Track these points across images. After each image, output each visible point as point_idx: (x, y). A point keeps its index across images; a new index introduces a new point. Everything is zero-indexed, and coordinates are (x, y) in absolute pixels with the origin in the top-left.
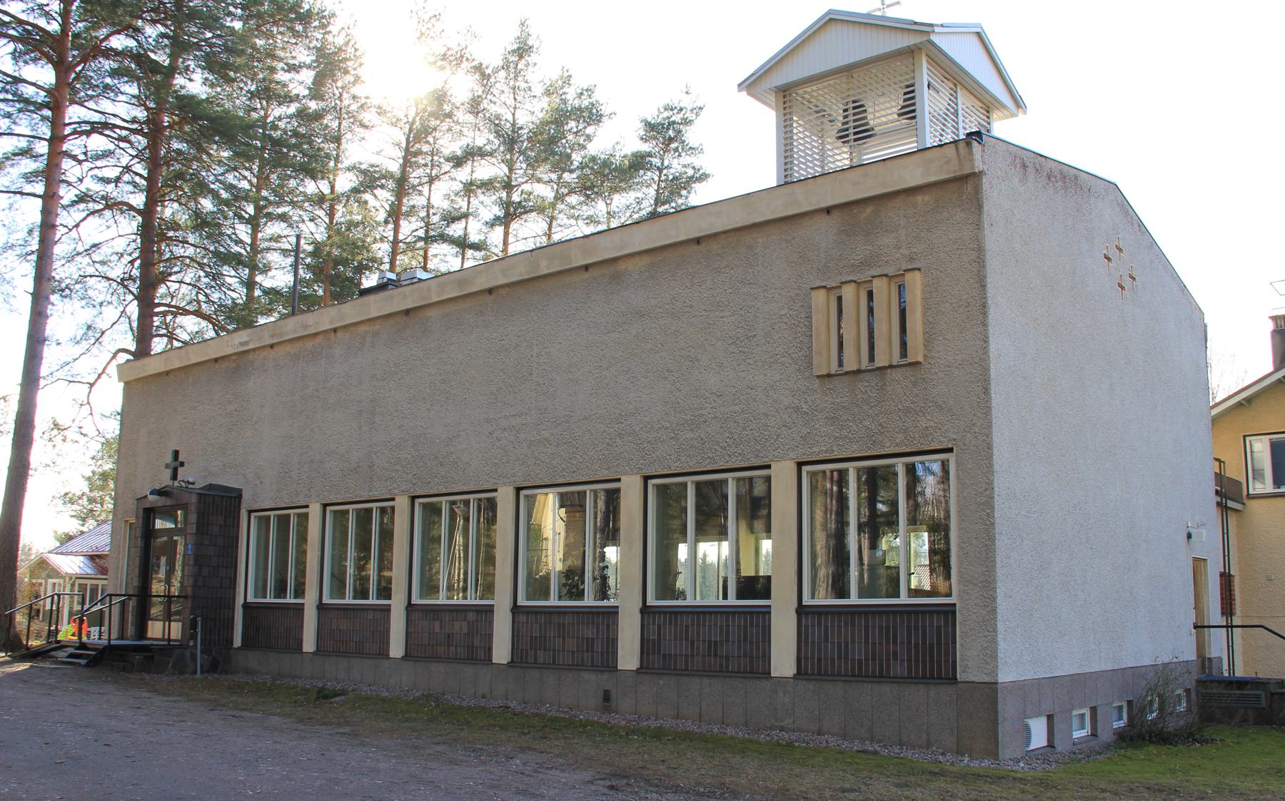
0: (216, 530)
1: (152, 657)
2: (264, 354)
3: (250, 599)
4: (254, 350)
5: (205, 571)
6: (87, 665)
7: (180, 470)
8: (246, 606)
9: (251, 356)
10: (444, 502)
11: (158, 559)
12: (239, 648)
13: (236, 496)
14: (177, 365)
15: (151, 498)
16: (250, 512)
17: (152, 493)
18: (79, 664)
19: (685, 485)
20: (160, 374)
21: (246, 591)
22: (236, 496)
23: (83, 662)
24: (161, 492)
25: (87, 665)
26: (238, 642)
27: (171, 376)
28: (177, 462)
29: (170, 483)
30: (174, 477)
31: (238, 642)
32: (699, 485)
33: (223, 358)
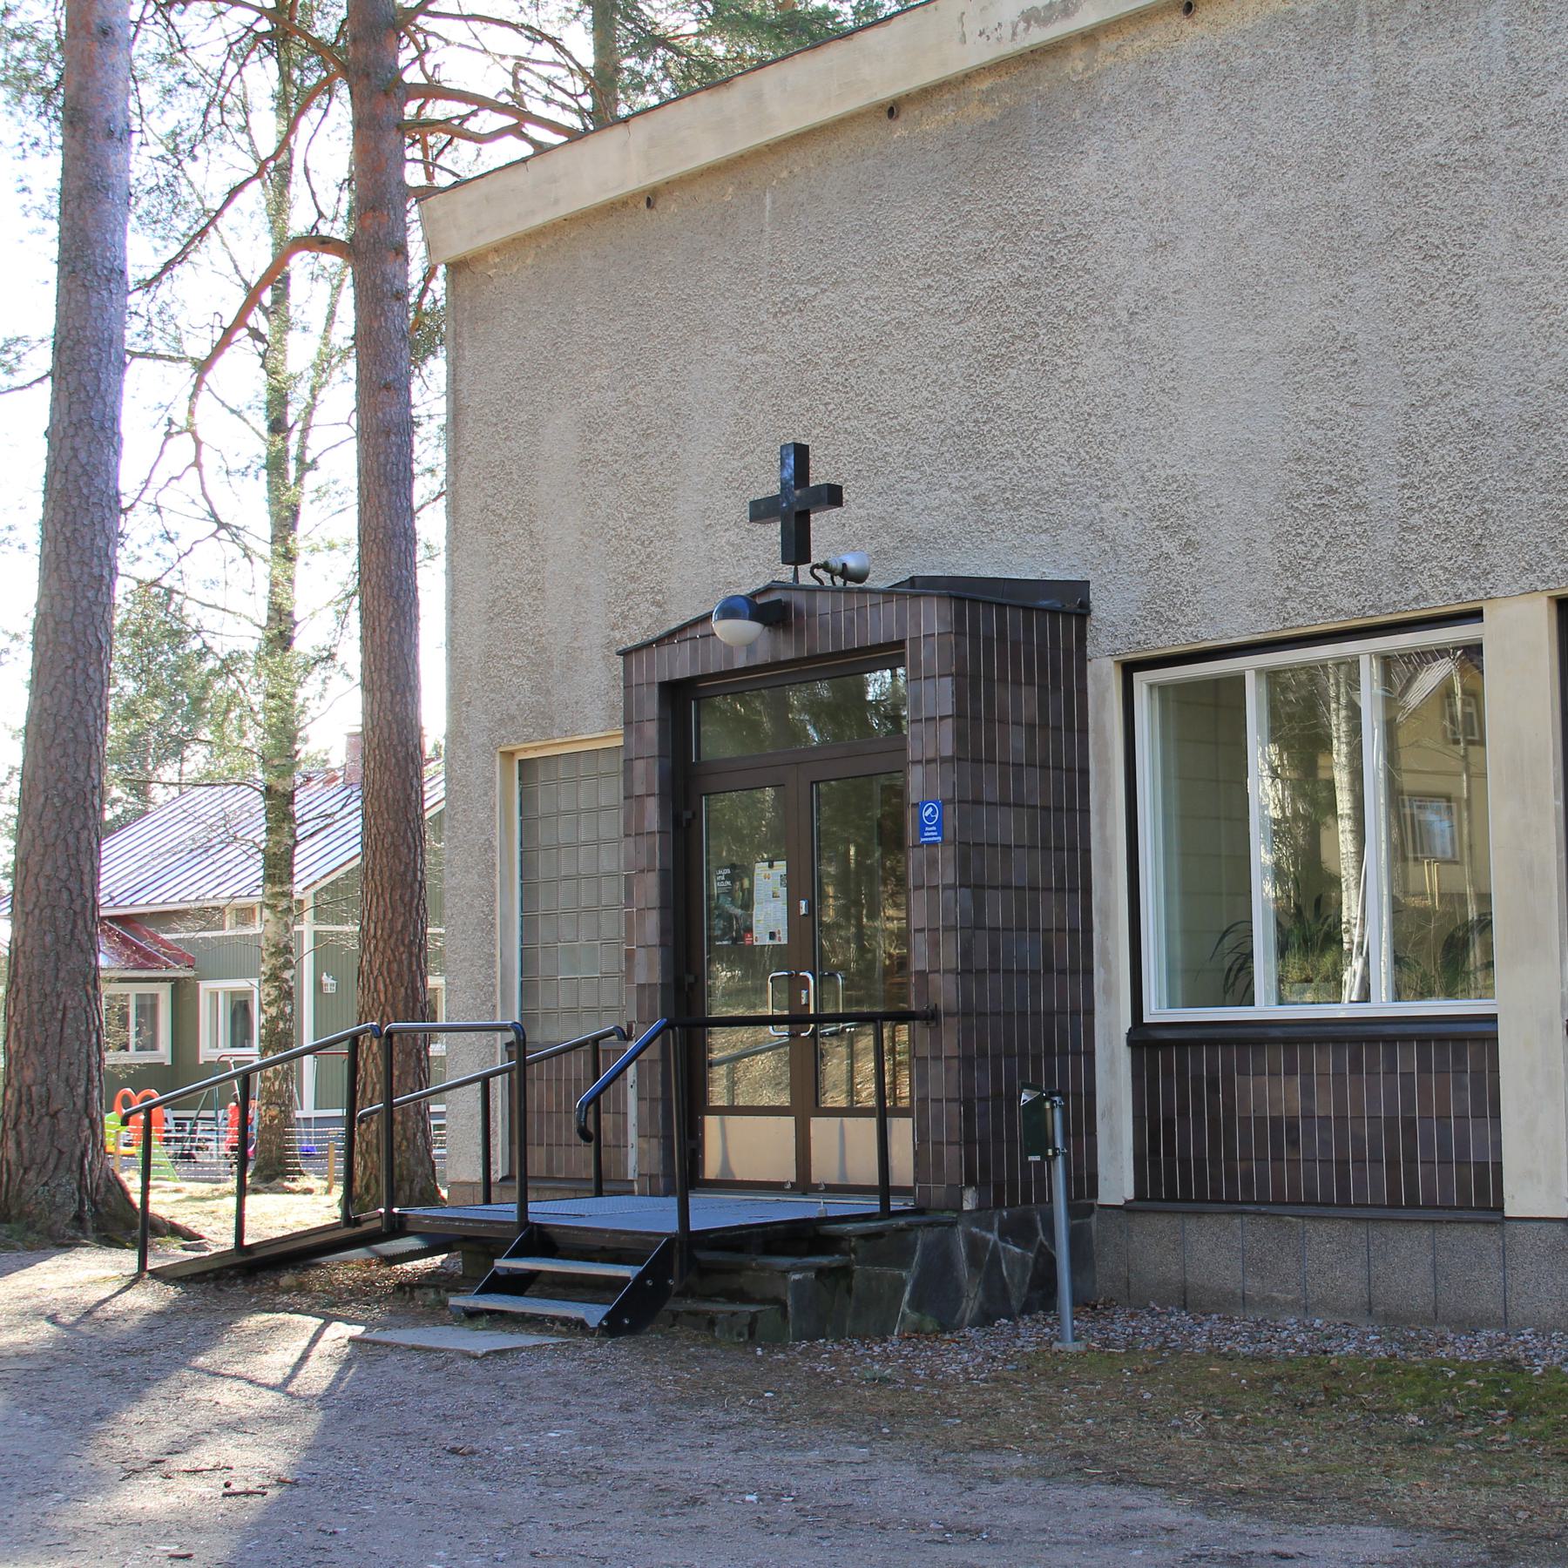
0: (1017, 741)
1: (845, 1271)
2: (1141, 44)
3: (1156, 1010)
4: (1088, 37)
5: (997, 910)
6: (612, 1328)
7: (822, 525)
8: (1144, 1039)
9: (1076, 63)
10: (1330, 663)
11: (740, 872)
12: (1127, 1209)
13: (1066, 607)
14: (710, 152)
15: (725, 630)
16: (1129, 669)
17: (729, 610)
18: (581, 1324)
19: (1238, 681)
20: (614, 209)
21: (1135, 977)
22: (1066, 607)
23: (594, 1314)
24: (770, 610)
25: (612, 1328)
26: (1117, 1180)
27: (670, 207)
28: (797, 505)
29: (786, 574)
30: (797, 548)
31: (1117, 1180)
32: (1272, 677)
33: (927, 94)
